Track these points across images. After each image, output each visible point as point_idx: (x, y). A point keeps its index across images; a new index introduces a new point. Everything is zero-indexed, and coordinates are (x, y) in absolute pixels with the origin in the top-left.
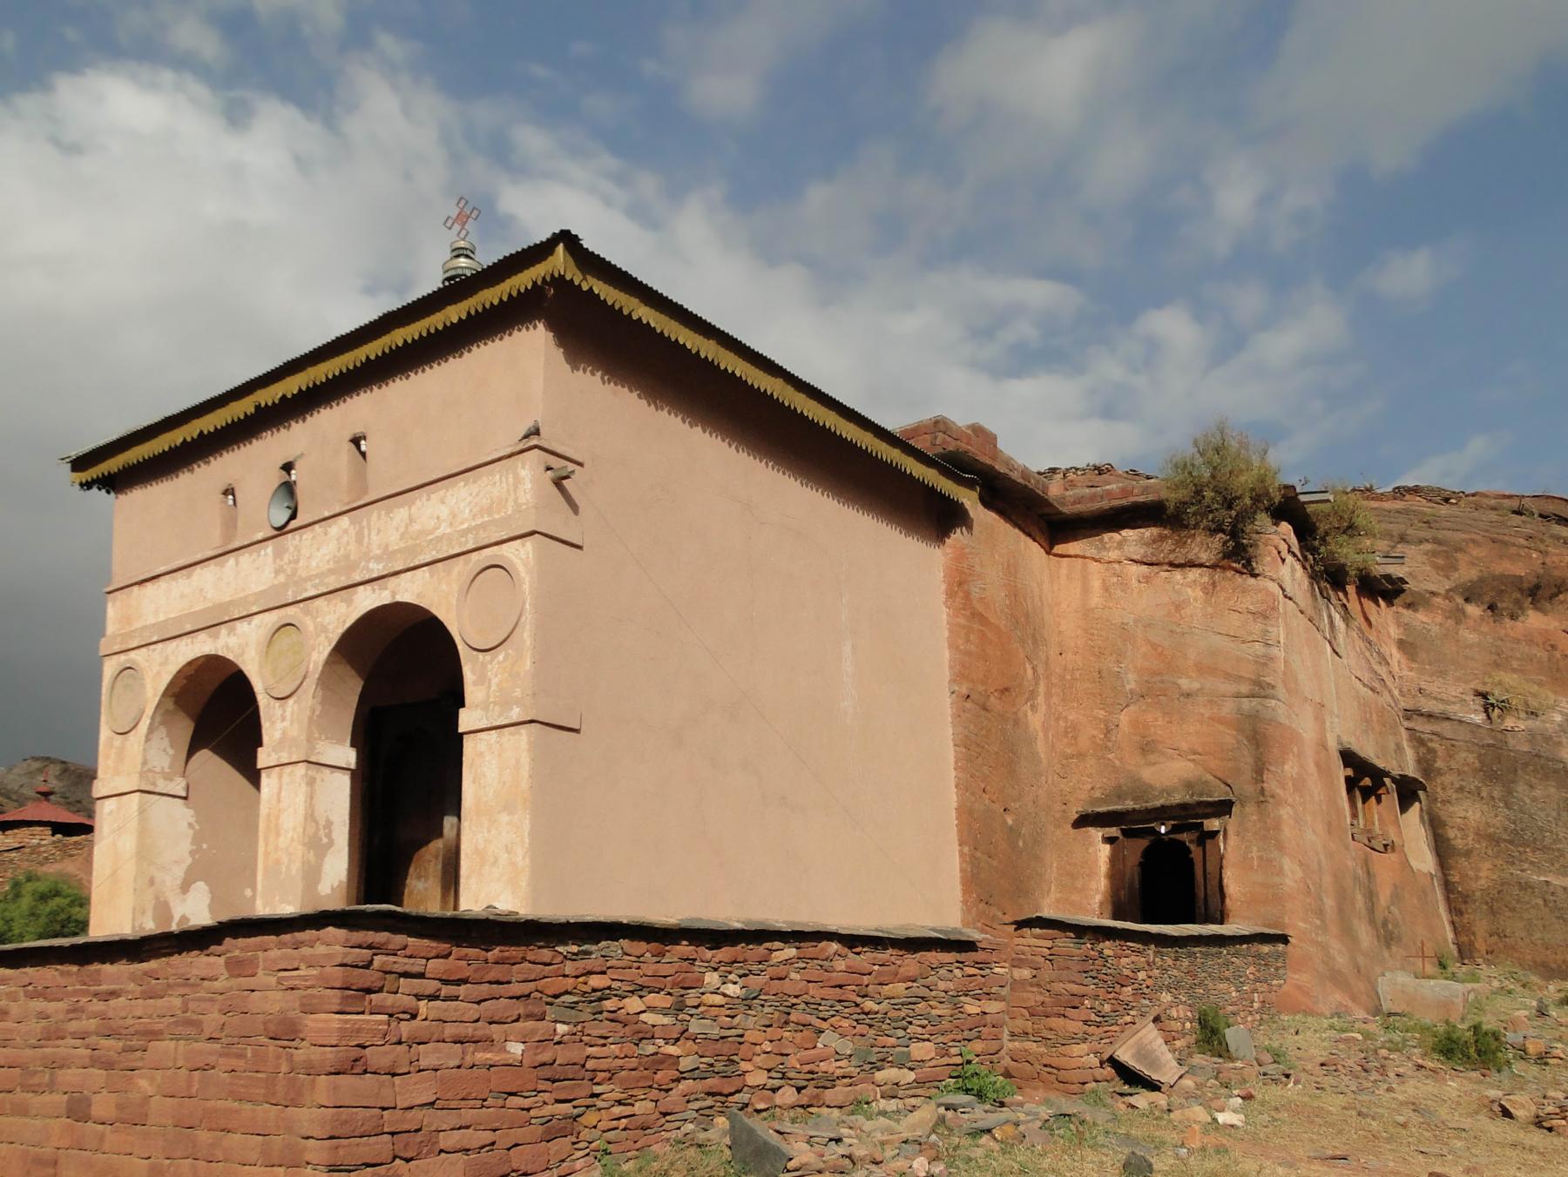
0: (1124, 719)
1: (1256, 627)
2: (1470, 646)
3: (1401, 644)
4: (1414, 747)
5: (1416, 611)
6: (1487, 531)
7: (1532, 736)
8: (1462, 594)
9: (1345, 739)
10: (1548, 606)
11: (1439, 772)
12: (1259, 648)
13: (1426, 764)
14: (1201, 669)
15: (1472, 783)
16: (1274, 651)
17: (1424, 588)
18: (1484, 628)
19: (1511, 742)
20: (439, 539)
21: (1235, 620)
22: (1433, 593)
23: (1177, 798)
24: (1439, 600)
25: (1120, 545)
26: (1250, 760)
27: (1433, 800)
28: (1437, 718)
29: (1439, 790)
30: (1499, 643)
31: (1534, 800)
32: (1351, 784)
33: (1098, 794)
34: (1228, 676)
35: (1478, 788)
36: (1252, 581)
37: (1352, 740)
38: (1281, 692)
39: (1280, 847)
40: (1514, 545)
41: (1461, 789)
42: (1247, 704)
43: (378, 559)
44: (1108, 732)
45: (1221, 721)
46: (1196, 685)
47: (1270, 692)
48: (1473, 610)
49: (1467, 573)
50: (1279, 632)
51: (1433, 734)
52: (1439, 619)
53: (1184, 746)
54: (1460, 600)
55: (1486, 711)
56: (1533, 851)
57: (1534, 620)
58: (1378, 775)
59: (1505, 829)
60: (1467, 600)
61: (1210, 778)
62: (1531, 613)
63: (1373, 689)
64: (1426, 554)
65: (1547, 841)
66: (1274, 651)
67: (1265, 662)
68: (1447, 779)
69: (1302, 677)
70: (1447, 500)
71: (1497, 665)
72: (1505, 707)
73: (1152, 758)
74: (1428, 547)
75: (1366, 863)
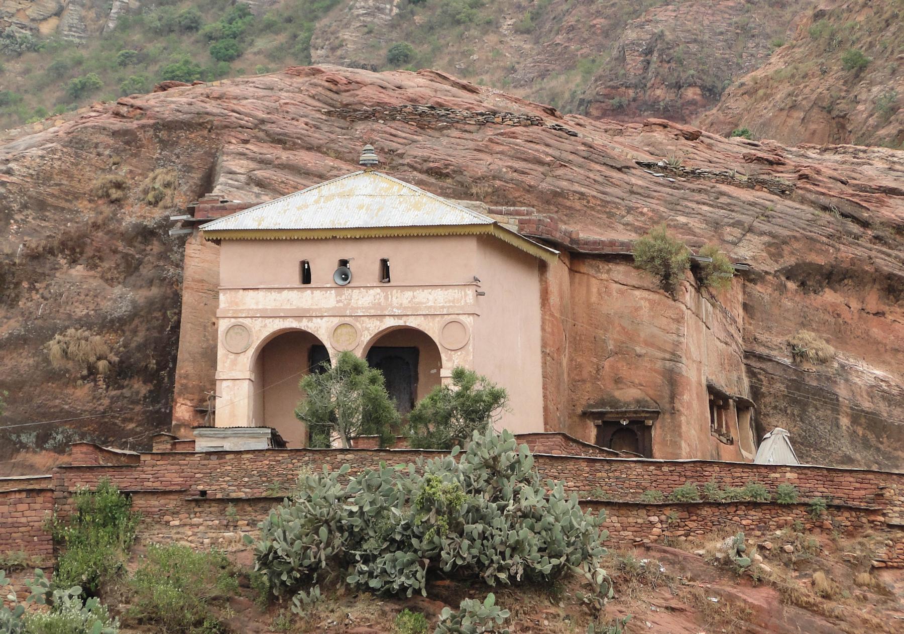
0: (607, 364)
1: (674, 326)
2: (787, 310)
3: (745, 306)
4: (749, 377)
5: (755, 284)
6: (804, 229)
7: (819, 376)
8: (784, 274)
9: (710, 378)
10: (837, 286)
11: (763, 395)
12: (675, 337)
13: (755, 391)
14: (647, 344)
15: (783, 404)
16: (682, 339)
17: (762, 268)
18: (797, 299)
19: (807, 379)
20: (430, 307)
21: (664, 321)
22: (767, 273)
23: (632, 408)
24: (770, 277)
25: (608, 271)
26: (668, 392)
27: (758, 412)
28: (764, 359)
29: (763, 407)
30: (806, 309)
31: (818, 418)
32: (712, 404)
33: (592, 402)
34: (659, 349)
35: (786, 407)
36: (671, 302)
37: (714, 377)
38: (684, 360)
39: (680, 435)
40: (819, 242)
41: (775, 408)
42: (668, 364)
43: (398, 308)
44: (598, 370)
45: (656, 371)
46: (644, 351)
47: (679, 359)
48: (791, 285)
49: (789, 261)
50: (684, 330)
51: (761, 369)
52: (770, 290)
53: (637, 381)
54: (783, 278)
55: (794, 357)
56: (815, 450)
57: (829, 296)
58: (726, 398)
59: (799, 435)
60: (788, 278)
61: (648, 399)
62: (827, 290)
63: (726, 343)
64: (764, 244)
65: (823, 445)
66: (682, 339)
67: (677, 344)
68: (768, 400)
69: (692, 349)
70: (783, 192)
71: (803, 325)
72: (803, 355)
73: (620, 386)
74: (766, 239)
75: (717, 448)
